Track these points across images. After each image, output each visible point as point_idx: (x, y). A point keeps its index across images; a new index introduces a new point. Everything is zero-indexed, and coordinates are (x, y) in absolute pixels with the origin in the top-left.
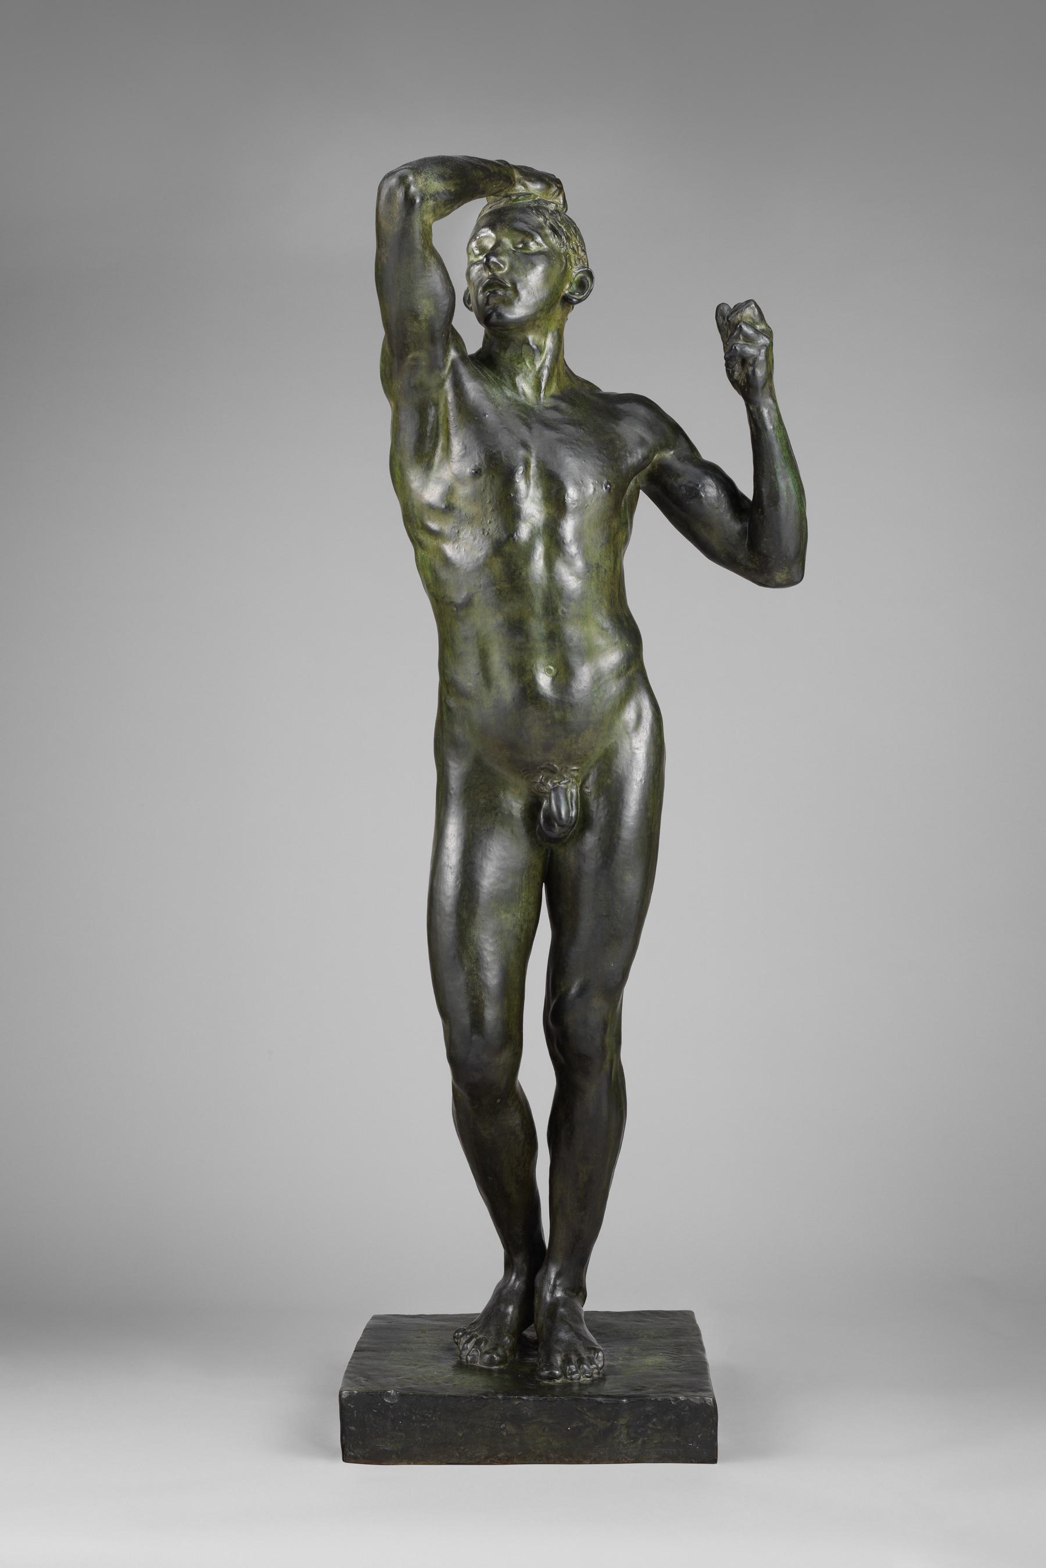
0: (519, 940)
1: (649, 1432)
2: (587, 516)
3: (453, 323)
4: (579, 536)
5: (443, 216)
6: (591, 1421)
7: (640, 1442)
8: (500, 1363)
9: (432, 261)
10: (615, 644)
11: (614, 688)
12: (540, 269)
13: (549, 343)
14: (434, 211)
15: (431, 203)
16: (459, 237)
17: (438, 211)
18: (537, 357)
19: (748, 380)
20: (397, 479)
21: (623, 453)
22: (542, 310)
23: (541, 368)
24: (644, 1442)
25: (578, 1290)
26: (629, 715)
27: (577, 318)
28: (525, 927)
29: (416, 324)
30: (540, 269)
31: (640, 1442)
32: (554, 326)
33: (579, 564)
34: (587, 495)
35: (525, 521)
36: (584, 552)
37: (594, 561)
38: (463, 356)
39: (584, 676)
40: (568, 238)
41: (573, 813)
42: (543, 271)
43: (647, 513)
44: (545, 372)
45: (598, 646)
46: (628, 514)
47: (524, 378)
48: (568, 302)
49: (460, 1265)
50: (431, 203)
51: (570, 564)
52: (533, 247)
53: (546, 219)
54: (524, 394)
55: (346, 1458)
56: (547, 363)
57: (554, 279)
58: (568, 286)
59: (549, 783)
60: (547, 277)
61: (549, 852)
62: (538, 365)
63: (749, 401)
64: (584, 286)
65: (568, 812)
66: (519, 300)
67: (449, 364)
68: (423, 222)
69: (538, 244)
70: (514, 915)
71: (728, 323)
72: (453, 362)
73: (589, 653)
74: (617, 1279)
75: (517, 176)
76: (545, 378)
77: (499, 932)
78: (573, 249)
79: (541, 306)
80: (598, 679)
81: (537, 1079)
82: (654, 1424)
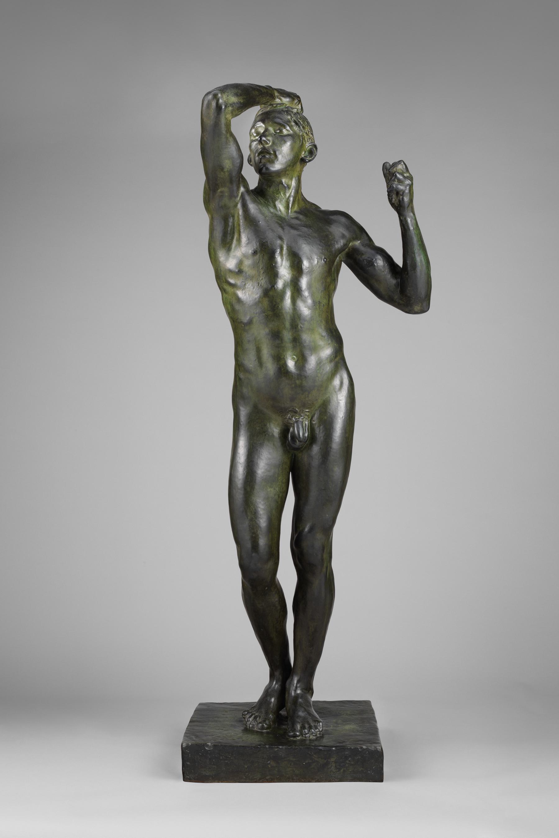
0: (277, 502)
1: (347, 765)
2: (314, 276)
3: (242, 173)
4: (310, 286)
5: (236, 115)
6: (316, 759)
7: (342, 771)
8: (267, 728)
9: (231, 139)
10: (329, 344)
11: (328, 368)
12: (289, 144)
13: (293, 183)
14: (232, 113)
15: (230, 108)
16: (245, 127)
17: (234, 113)
18: (287, 191)
19: (400, 203)
20: (212, 256)
21: (333, 242)
22: (289, 166)
23: (289, 197)
24: (344, 771)
25: (309, 689)
26: (336, 382)
27: (309, 170)
28: (281, 495)
29: (222, 173)
30: (289, 144)
31: (342, 771)
32: (296, 174)
33: (310, 301)
34: (314, 264)
35: (281, 278)
36: (312, 295)
37: (317, 300)
38: (247, 190)
39: (312, 361)
40: (303, 127)
41: (306, 435)
42: (290, 145)
43: (346, 274)
44: (291, 199)
45: (320, 345)
46: (336, 275)
47: (280, 202)
48: (303, 161)
49: (246, 676)
50: (230, 108)
51: (304, 301)
52: (285, 132)
53: (292, 117)
54: (280, 211)
55: (185, 779)
56: (292, 194)
57: (296, 149)
58: (303, 153)
59: (293, 419)
60: (292, 148)
61: (293, 455)
62: (288, 195)
63: (400, 214)
64: (312, 153)
65: (304, 434)
66: (277, 160)
67: (240, 195)
68: (226, 119)
69: (287, 130)
70: (274, 489)
71: (389, 172)
72: (242, 193)
73: (315, 349)
74: (330, 683)
75: (276, 94)
76: (291, 202)
77: (267, 498)
78: (306, 133)
79: (289, 164)
80: (319, 363)
81: (287, 577)
82: (349, 761)
